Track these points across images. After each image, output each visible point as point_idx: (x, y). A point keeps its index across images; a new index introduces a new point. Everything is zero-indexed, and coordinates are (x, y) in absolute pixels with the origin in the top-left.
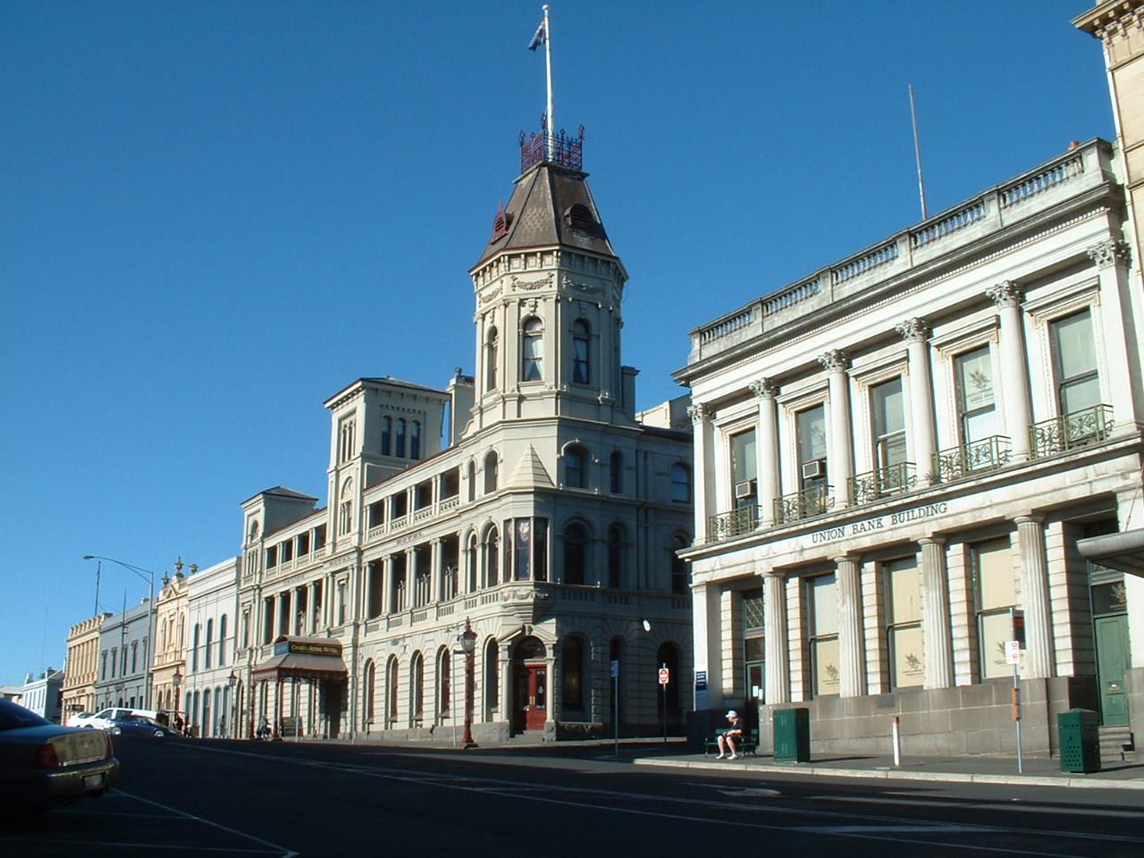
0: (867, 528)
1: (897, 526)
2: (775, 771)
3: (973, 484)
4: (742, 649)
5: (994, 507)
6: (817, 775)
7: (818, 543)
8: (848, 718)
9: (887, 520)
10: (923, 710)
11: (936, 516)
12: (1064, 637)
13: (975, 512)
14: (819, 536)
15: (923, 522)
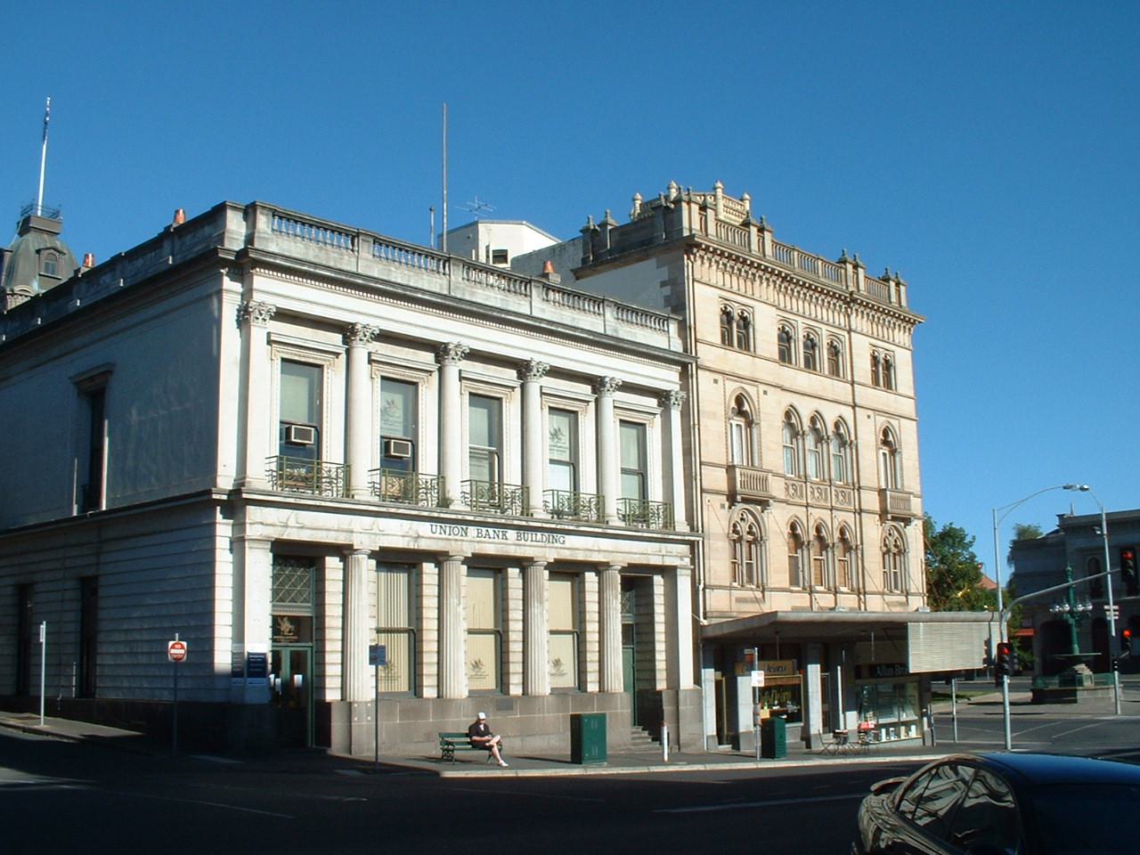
0: (492, 536)
1: (520, 542)
2: (615, 772)
3: (600, 530)
4: (316, 629)
5: (602, 553)
6: (653, 772)
7: (437, 535)
8: (465, 719)
9: (511, 534)
10: (539, 713)
11: (556, 545)
12: (332, 652)
13: (587, 552)
14: (439, 527)
15: (545, 547)
